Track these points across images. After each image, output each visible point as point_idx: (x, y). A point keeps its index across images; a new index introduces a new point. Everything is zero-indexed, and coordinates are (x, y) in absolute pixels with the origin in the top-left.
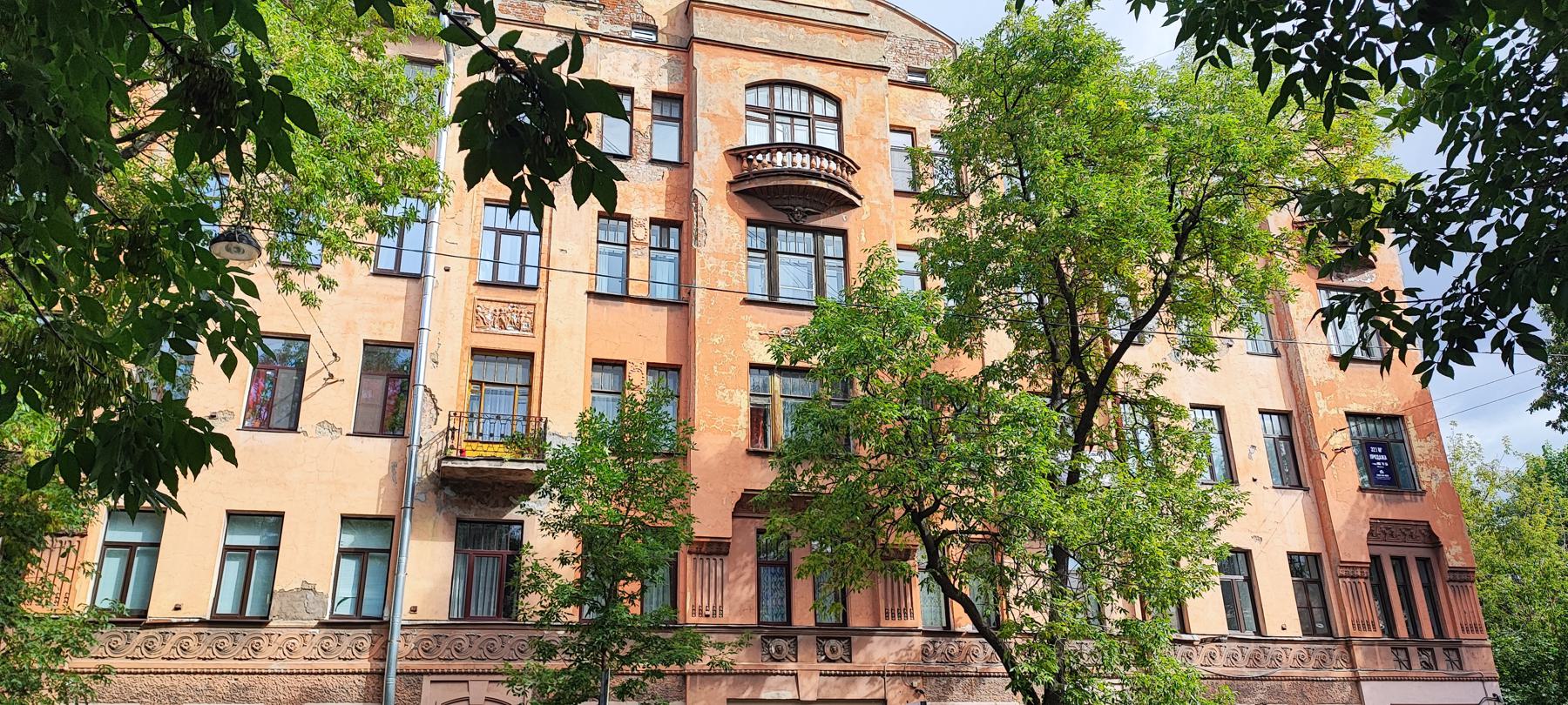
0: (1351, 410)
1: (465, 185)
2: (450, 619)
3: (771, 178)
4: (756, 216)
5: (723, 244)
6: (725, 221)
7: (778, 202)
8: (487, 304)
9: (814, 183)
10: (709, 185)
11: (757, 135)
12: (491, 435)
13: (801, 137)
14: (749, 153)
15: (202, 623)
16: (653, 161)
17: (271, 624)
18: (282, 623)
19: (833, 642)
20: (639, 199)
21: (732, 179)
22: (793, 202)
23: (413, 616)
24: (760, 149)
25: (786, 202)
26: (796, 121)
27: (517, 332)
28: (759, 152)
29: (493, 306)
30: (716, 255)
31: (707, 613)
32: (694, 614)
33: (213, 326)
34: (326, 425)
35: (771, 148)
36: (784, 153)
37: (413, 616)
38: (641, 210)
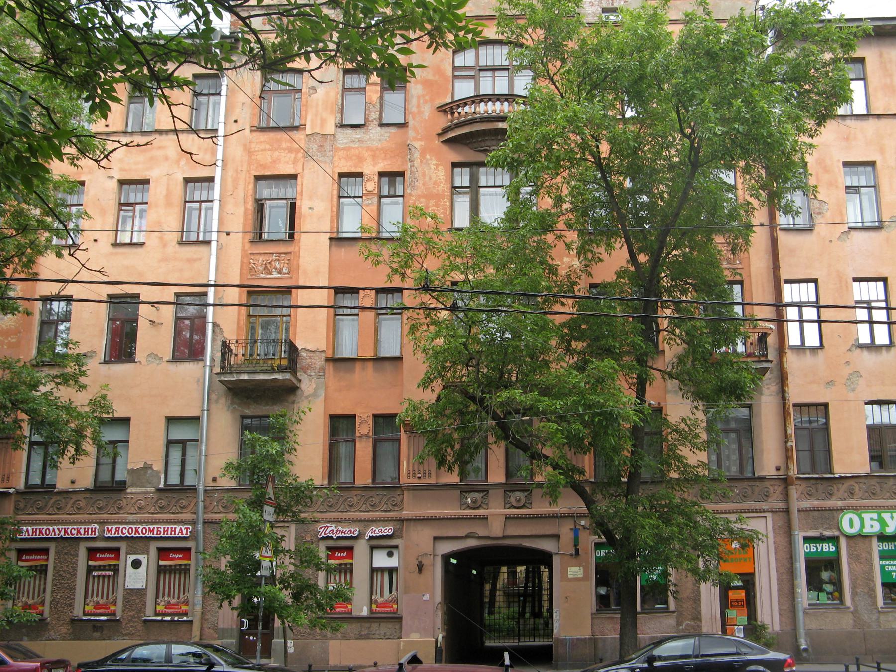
0: (340, 412)
1: (298, 176)
2: (240, 485)
3: (466, 127)
4: (458, 158)
5: (431, 186)
6: (433, 167)
7: (476, 145)
8: (257, 257)
9: (482, 108)
10: (421, 140)
11: (465, 89)
12: (266, 355)
13: (502, 87)
14: (459, 106)
15: (87, 490)
16: (382, 125)
17: (129, 490)
18: (134, 490)
19: (518, 494)
20: (369, 160)
21: (440, 132)
22: (488, 143)
23: (214, 484)
24: (464, 102)
25: (483, 144)
26: (497, 73)
27: (280, 276)
28: (466, 104)
29: (261, 259)
30: (424, 196)
31: (419, 476)
32: (409, 477)
33: (659, 304)
34: (153, 356)
35: (478, 98)
36: (494, 102)
37: (214, 484)
38: (371, 167)
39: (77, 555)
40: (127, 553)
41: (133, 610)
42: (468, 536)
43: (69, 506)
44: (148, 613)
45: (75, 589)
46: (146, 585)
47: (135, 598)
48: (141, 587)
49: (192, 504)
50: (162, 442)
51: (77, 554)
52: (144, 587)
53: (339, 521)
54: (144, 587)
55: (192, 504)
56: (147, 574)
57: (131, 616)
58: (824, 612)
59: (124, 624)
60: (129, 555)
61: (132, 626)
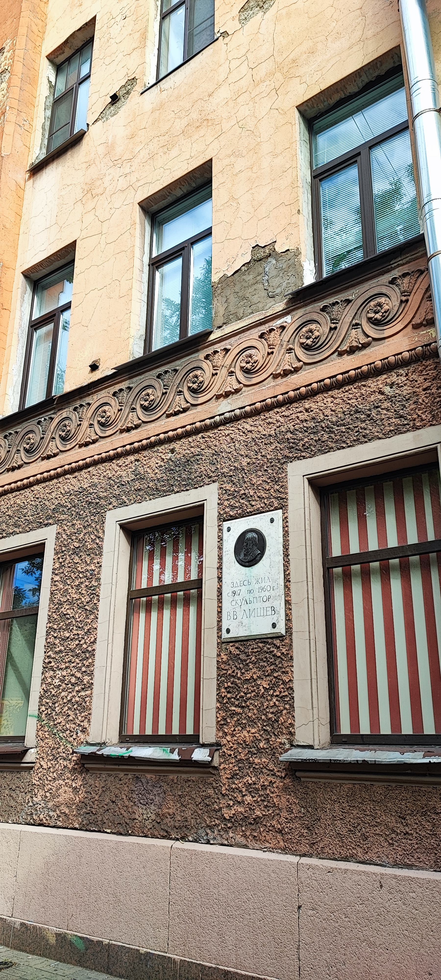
39: (99, 551)
40: (223, 518)
41: (252, 722)
42: (22, 312)
43: (85, 424)
44: (301, 737)
45: (92, 654)
46: (288, 620)
47: (253, 672)
48: (267, 630)
49: (415, 299)
50: (305, 175)
51: (100, 547)
52: (281, 629)
53: (402, 260)
54: (281, 629)
55: (415, 299)
56: (287, 579)
57: (244, 744)
58: (165, 37)
59: (224, 776)
60: (226, 525)
61: (250, 788)
